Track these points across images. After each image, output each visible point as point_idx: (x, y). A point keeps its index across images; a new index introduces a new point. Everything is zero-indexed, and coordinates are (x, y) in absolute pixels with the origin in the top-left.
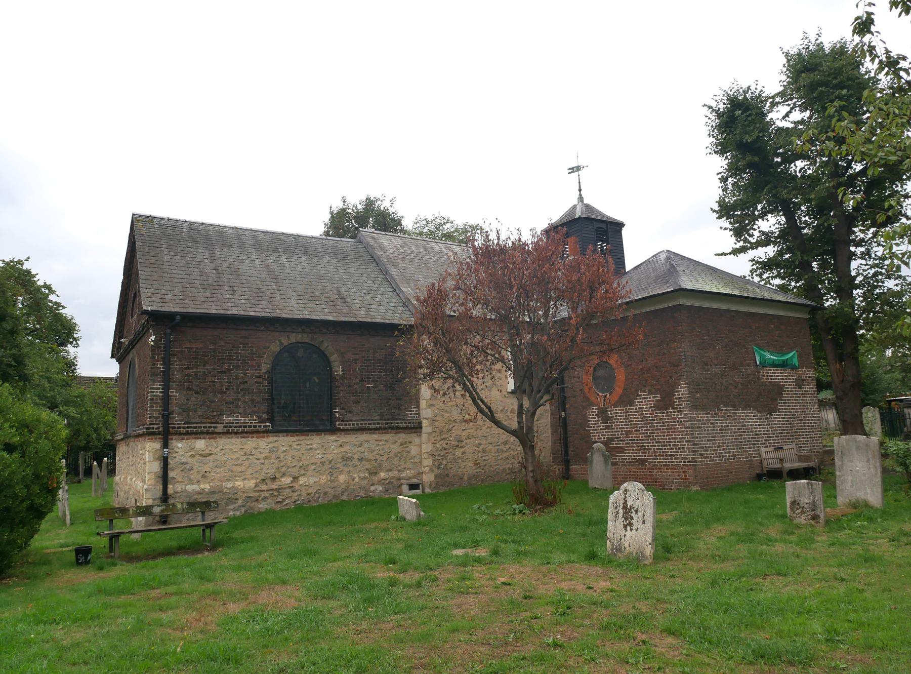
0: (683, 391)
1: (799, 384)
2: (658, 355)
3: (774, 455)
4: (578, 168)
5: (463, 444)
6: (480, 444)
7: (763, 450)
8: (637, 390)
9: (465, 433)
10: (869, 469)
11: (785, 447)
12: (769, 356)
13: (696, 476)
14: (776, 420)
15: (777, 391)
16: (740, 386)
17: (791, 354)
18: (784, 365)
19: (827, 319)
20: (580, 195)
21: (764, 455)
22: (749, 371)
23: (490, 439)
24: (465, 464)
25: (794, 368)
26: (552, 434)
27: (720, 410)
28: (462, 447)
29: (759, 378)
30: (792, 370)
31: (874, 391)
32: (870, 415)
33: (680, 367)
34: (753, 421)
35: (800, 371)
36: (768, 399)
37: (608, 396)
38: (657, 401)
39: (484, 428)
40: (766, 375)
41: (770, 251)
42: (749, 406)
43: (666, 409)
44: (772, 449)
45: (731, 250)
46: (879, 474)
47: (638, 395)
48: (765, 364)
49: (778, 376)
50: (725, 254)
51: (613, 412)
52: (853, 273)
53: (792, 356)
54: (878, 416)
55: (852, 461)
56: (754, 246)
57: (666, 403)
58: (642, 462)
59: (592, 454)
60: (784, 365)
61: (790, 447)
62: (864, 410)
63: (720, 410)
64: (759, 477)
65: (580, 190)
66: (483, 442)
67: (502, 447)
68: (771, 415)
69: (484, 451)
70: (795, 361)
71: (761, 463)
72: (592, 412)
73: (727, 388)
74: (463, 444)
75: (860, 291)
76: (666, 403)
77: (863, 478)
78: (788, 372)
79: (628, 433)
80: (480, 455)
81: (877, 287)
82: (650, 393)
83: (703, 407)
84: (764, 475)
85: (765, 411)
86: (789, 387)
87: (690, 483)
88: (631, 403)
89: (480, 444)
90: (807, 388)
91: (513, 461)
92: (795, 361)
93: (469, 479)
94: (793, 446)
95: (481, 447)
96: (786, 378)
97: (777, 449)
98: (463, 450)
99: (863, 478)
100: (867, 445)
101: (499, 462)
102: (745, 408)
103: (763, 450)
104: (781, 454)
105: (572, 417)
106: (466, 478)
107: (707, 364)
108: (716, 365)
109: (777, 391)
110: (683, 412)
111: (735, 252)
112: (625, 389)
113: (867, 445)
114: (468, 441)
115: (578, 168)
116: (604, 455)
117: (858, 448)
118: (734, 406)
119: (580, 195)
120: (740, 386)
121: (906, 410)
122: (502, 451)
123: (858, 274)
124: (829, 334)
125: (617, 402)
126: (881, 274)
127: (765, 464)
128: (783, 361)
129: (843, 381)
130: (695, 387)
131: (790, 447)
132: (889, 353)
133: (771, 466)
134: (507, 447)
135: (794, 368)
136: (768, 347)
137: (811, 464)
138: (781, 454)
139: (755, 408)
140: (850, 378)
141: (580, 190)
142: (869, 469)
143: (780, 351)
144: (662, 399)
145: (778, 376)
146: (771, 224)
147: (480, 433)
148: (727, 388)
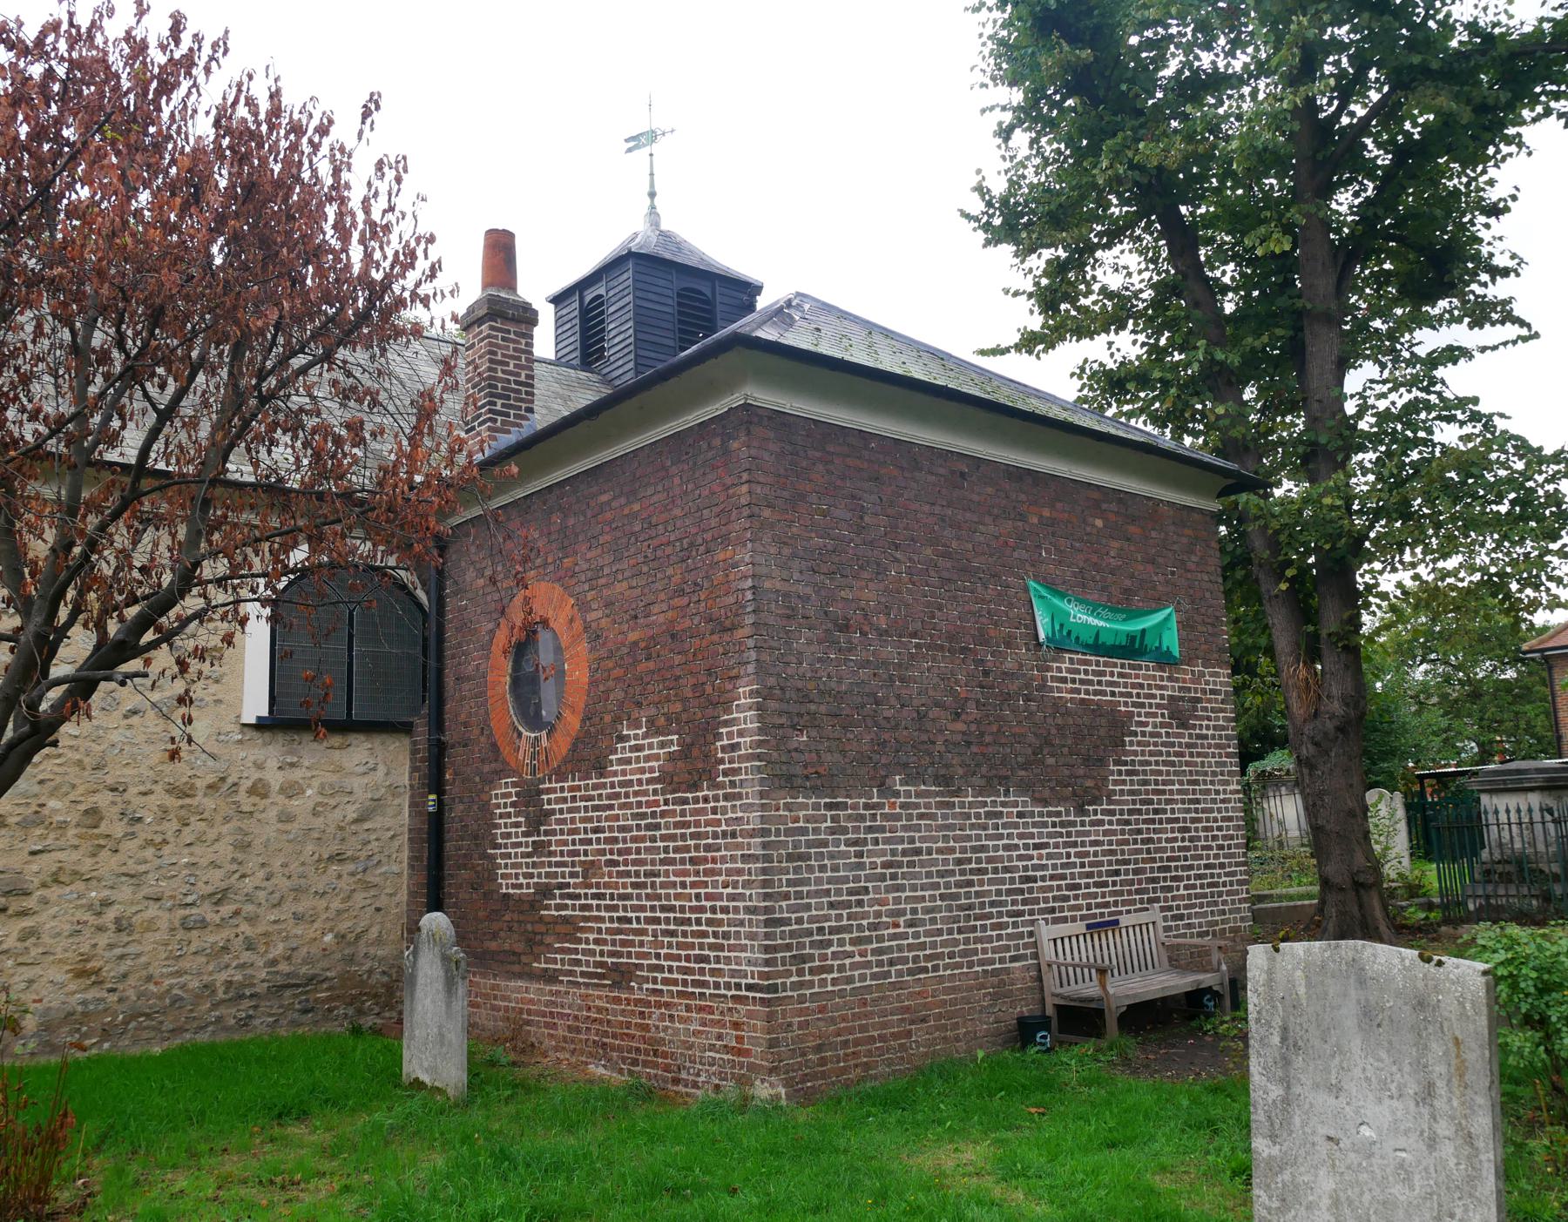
0: (743, 722)
1: (1181, 713)
2: (681, 592)
3: (1085, 951)
4: (652, 136)
5: (30, 903)
6: (106, 903)
7: (1047, 932)
8: (617, 720)
9: (47, 863)
10: (1432, 1142)
11: (1125, 920)
12: (1081, 617)
13: (773, 1044)
14: (1099, 830)
15: (1105, 732)
16: (971, 709)
17: (1158, 617)
18: (1132, 649)
19: (1277, 532)
20: (653, 207)
21: (1048, 952)
22: (1010, 664)
23: (151, 885)
24: (28, 973)
25: (1165, 661)
26: (411, 867)
27: (886, 791)
28: (24, 913)
29: (1043, 687)
30: (1161, 666)
31: (1391, 753)
32: (1383, 810)
33: (740, 633)
34: (1017, 833)
35: (1186, 674)
36: (1071, 758)
37: (544, 743)
38: (671, 757)
39: (130, 846)
40: (1070, 680)
41: (1127, 346)
42: (1003, 780)
43: (695, 787)
44: (1080, 927)
45: (1016, 338)
46: (1489, 1184)
47: (622, 738)
48: (1061, 645)
49: (1115, 683)
50: (1007, 350)
51: (555, 795)
52: (1350, 408)
53: (1162, 624)
54: (1401, 813)
55: (1336, 1090)
56: (1083, 331)
57: (692, 769)
58: (621, 976)
59: (415, 953)
60: (1132, 649)
61: (1143, 917)
62: (1371, 796)
63: (886, 791)
64: (1025, 1031)
65: (652, 195)
66: (125, 892)
67: (206, 911)
68: (1081, 811)
69: (121, 926)
70: (1171, 641)
71: (1040, 979)
72: (504, 794)
73: (921, 717)
74: (30, 903)
75: (1369, 457)
76: (692, 769)
77: (1398, 1191)
78: (1147, 672)
79: (590, 868)
80: (103, 940)
81: (1417, 442)
82: (654, 729)
83: (822, 782)
84: (1043, 1023)
85: (1061, 800)
86: (1150, 721)
87: (751, 1067)
88: (601, 770)
89: (106, 903)
90: (1205, 727)
91: (246, 956)
92: (1171, 641)
93: (47, 1027)
94: (1155, 914)
95: (111, 914)
96: (1140, 692)
97: (1098, 927)
98: (27, 923)
99: (1398, 1191)
100: (1421, 1004)
101: (185, 964)
102: (987, 788)
103: (1047, 932)
104: (1110, 947)
105: (459, 809)
106: (30, 1023)
107: (845, 628)
108: (882, 633)
109: (1105, 732)
110: (740, 804)
111: (1029, 343)
112: (587, 718)
113: (1421, 1004)
114: (54, 892)
115: (652, 136)
116: (445, 959)
117: (1369, 1016)
118: (944, 780)
119: (653, 207)
120: (971, 709)
121: (1485, 799)
122: (203, 924)
123: (1362, 410)
124: (1280, 577)
125: (565, 761)
126: (1429, 407)
127: (1051, 984)
128: (1131, 638)
129: (1316, 715)
130: (787, 710)
131: (1143, 917)
132: (1419, 673)
133: (1066, 990)
134: (226, 910)
135: (1165, 661)
136: (1079, 587)
137: (1207, 979)
138: (1110, 947)
139: (1025, 787)
140: (1336, 707)
141: (652, 195)
142: (1432, 1142)
143: (1124, 604)
144: (685, 753)
145: (1115, 683)
146: (1123, 268)
147: (108, 863)
148: (921, 717)
